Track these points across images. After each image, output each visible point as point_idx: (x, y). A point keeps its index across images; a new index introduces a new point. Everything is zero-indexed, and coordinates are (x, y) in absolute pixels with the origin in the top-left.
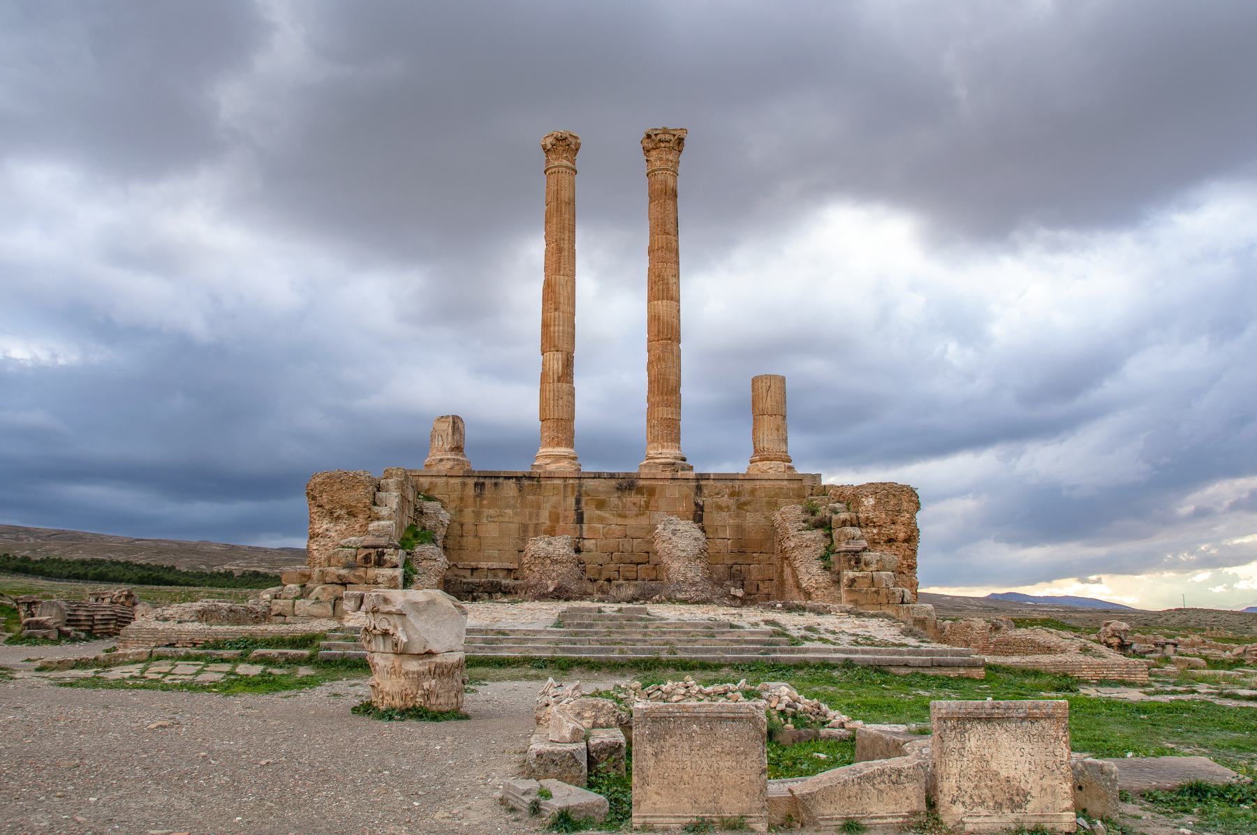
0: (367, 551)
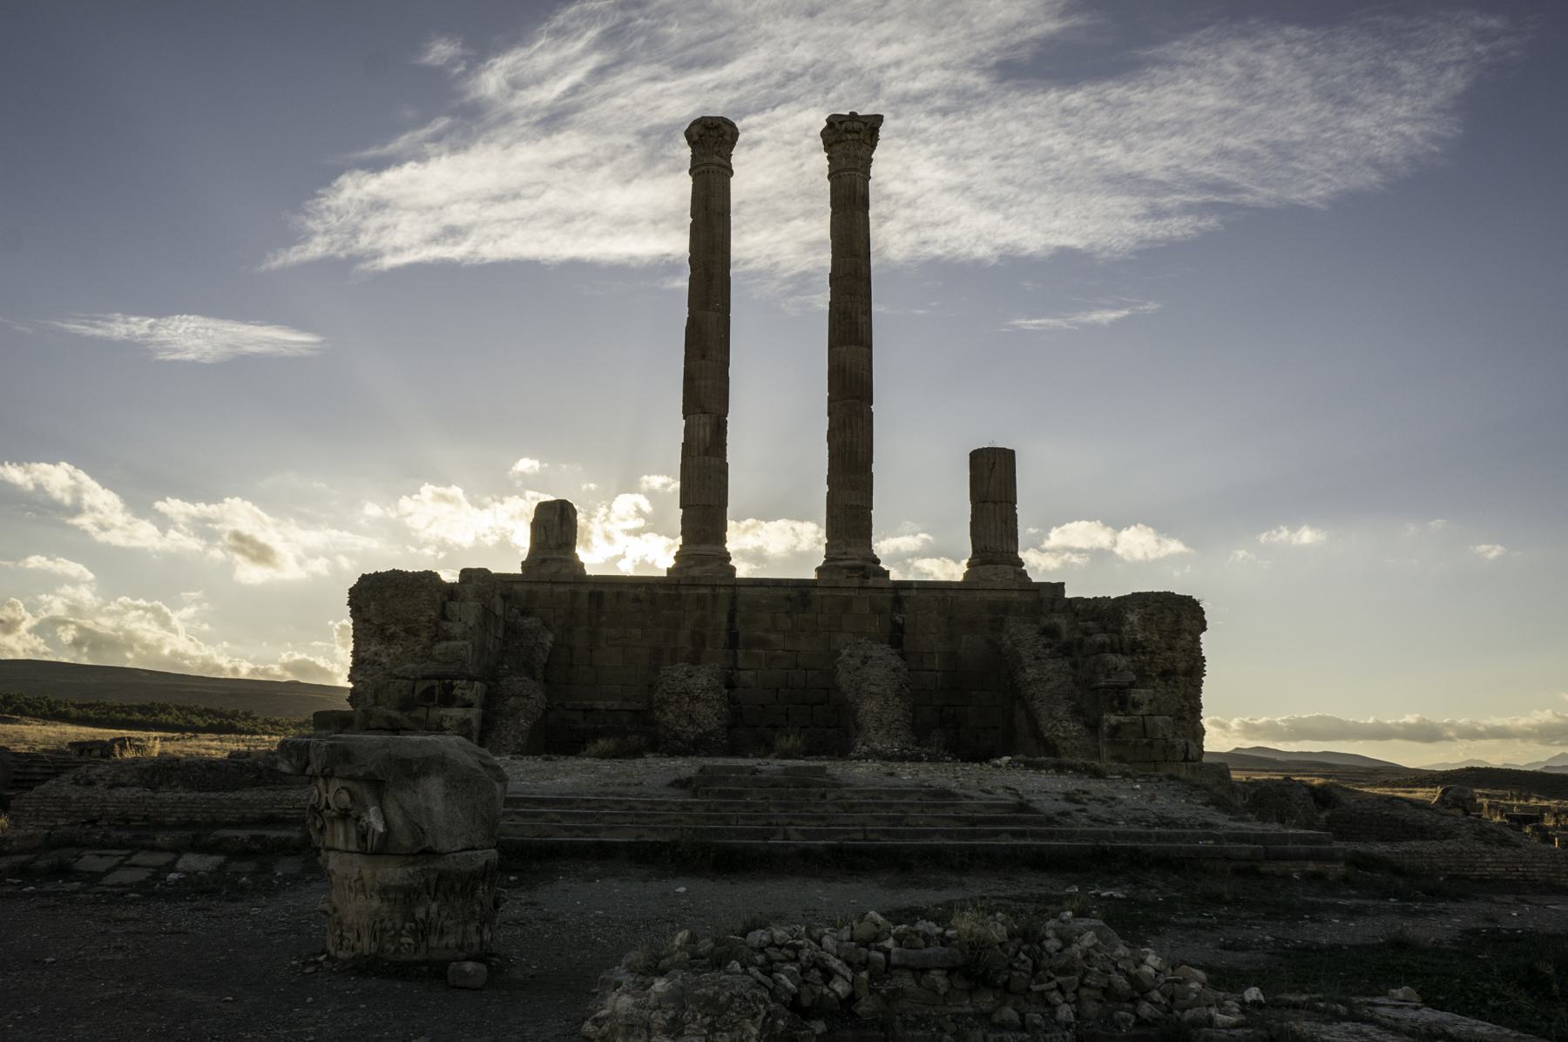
0: (428, 684)
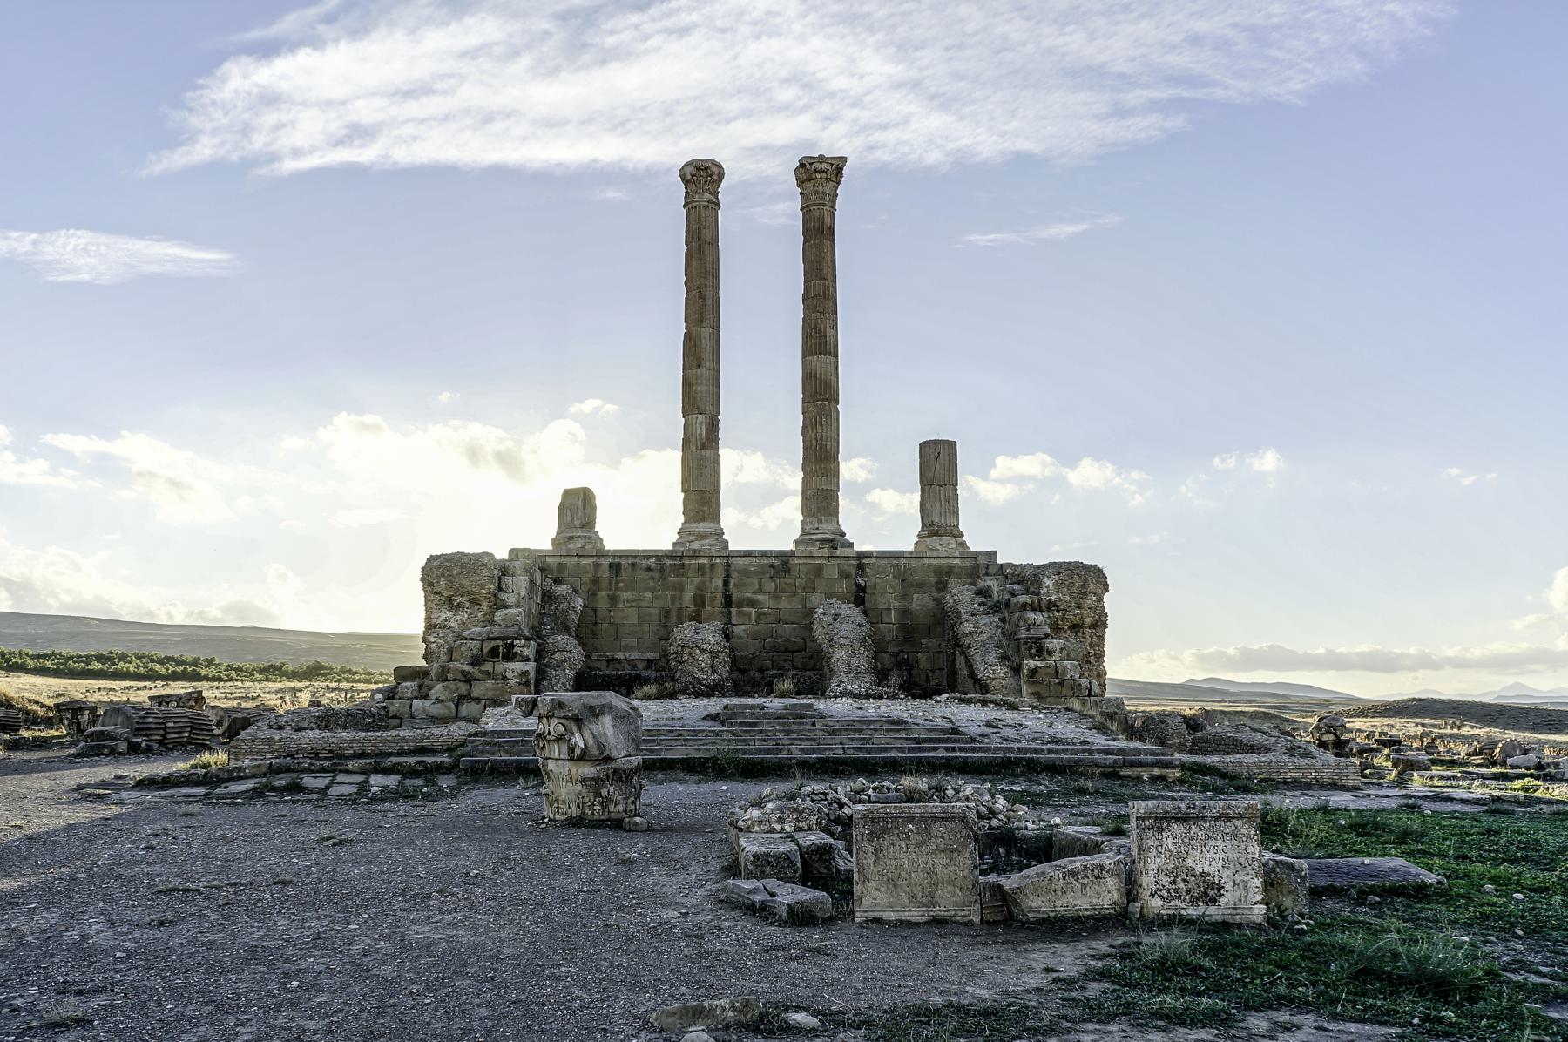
0: (493, 643)
